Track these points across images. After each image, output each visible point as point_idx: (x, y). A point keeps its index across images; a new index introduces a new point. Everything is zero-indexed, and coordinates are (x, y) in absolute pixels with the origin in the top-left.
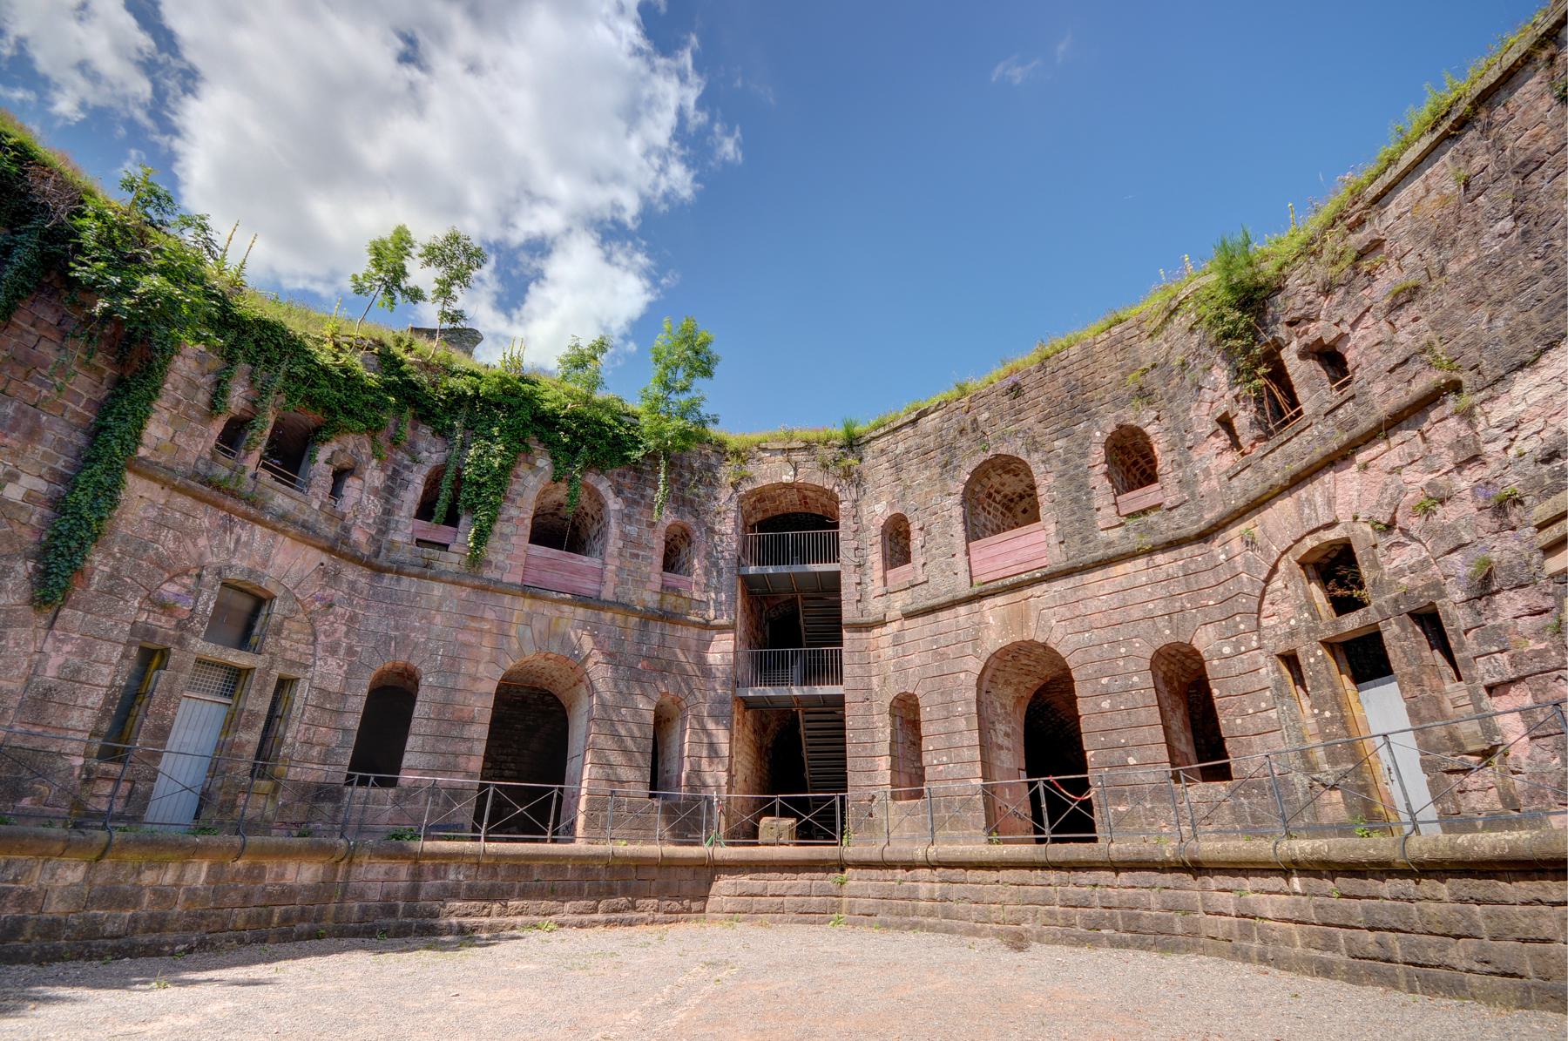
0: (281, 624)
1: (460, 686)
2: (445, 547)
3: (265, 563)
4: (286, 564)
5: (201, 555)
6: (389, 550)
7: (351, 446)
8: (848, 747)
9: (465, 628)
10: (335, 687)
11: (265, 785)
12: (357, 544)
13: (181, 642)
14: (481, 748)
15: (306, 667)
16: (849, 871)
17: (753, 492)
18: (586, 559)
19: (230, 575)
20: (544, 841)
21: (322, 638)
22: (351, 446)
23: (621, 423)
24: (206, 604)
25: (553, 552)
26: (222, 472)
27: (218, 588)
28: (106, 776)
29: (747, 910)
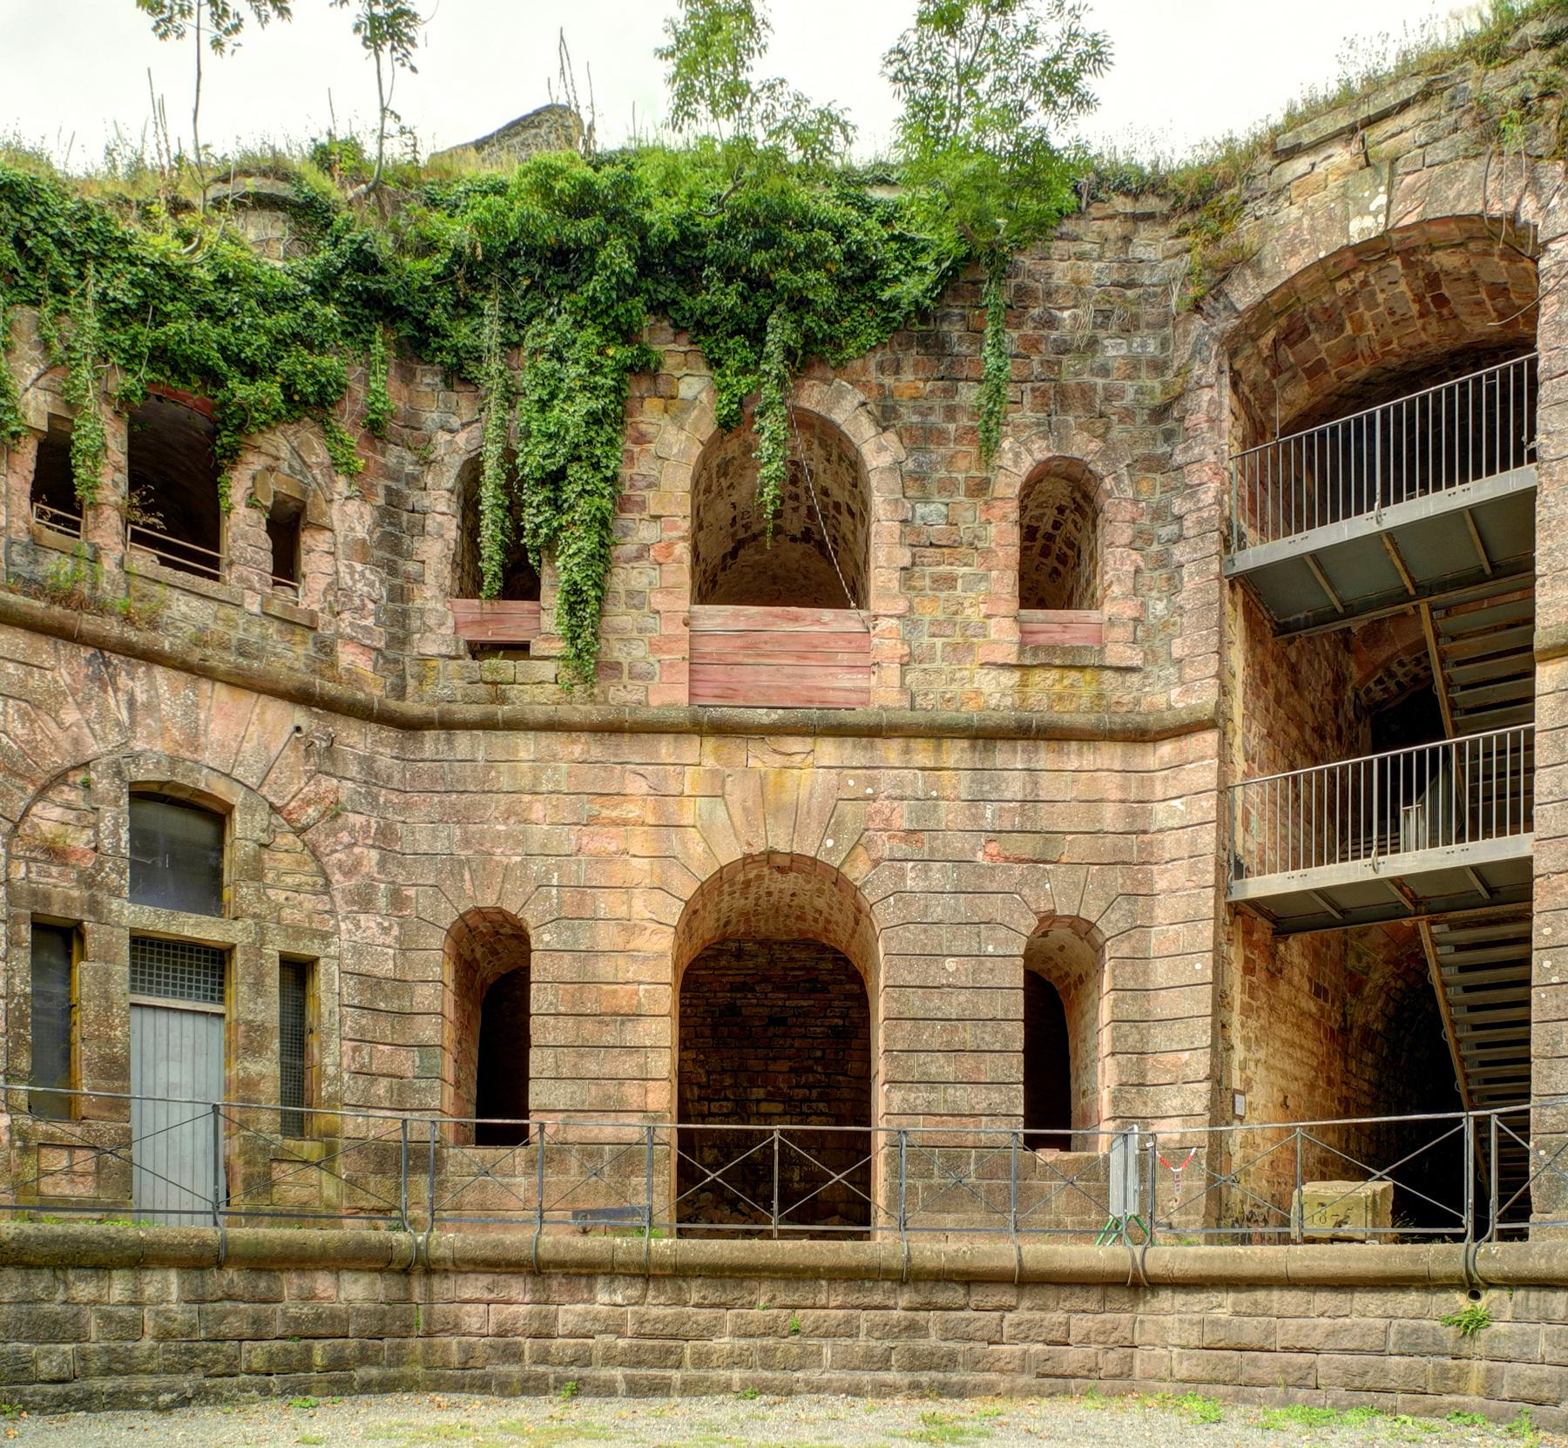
0: (258, 859)
1: (604, 944)
2: (519, 649)
3: (193, 739)
4: (235, 742)
5: (76, 742)
6: (421, 679)
7: (285, 452)
8: (1537, 996)
9: (593, 820)
10: (387, 968)
11: (310, 1149)
12: (355, 679)
13: (94, 907)
14: (664, 1063)
15: (325, 936)
16: (1489, 1297)
17: (1262, 312)
18: (827, 614)
19: (140, 774)
20: (768, 1235)
21: (337, 877)
22: (285, 452)
23: (867, 208)
24: (115, 833)
25: (752, 615)
26: (56, 566)
27: (124, 801)
28: (52, 1144)
29: (1230, 1373)
